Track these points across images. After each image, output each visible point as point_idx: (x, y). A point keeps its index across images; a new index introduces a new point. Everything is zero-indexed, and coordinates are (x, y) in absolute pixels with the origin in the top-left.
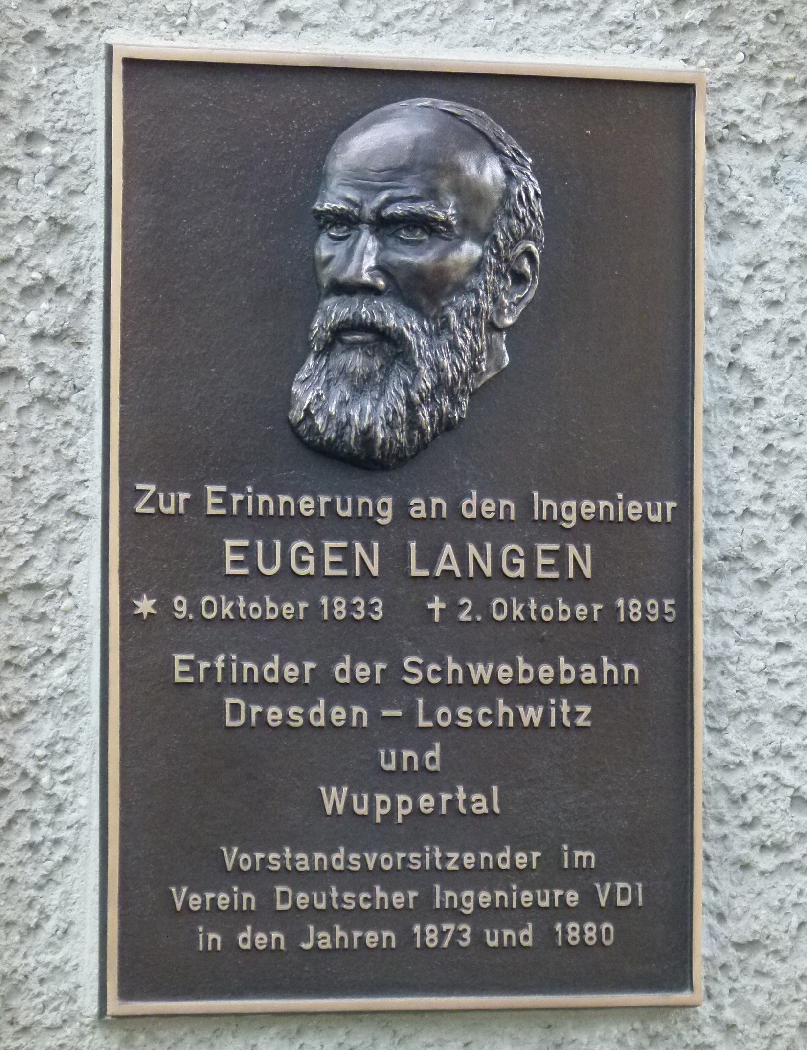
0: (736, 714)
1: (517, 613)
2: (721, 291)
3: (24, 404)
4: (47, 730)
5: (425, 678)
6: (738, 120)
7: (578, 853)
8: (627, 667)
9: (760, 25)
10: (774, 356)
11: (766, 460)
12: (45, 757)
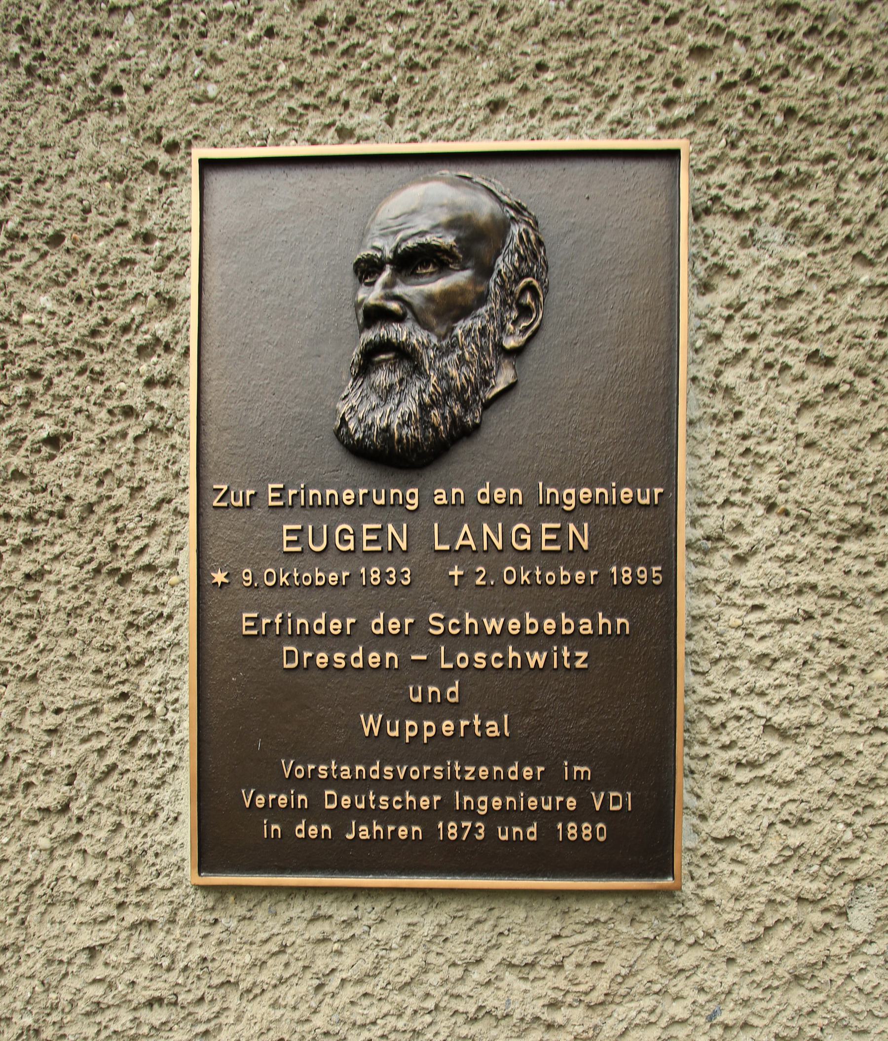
0: (716, 662)
1: (524, 578)
2: (705, 327)
3: (139, 433)
4: (159, 671)
5: (446, 630)
6: (721, 193)
7: (576, 768)
8: (619, 621)
9: (740, 115)
10: (751, 378)
11: (744, 461)
12: (160, 692)
